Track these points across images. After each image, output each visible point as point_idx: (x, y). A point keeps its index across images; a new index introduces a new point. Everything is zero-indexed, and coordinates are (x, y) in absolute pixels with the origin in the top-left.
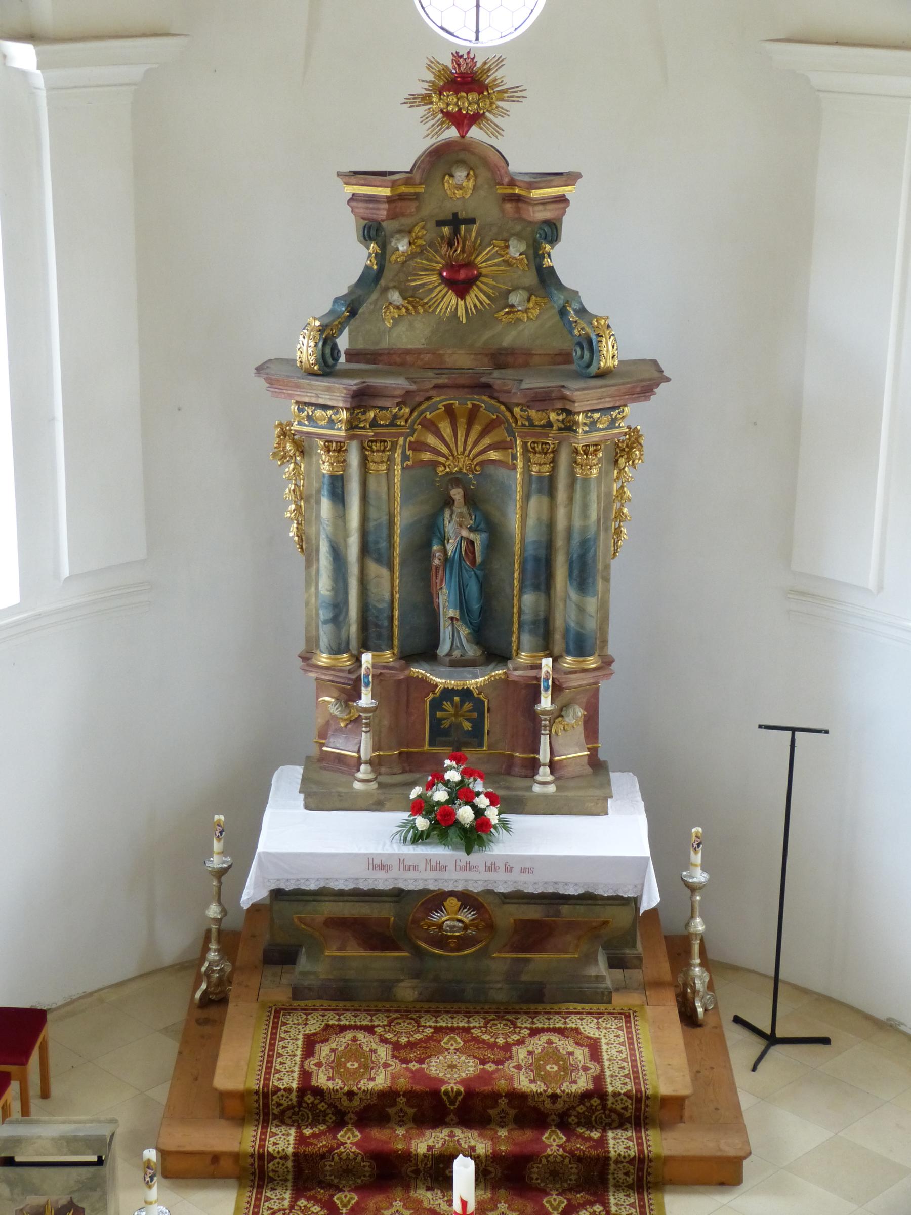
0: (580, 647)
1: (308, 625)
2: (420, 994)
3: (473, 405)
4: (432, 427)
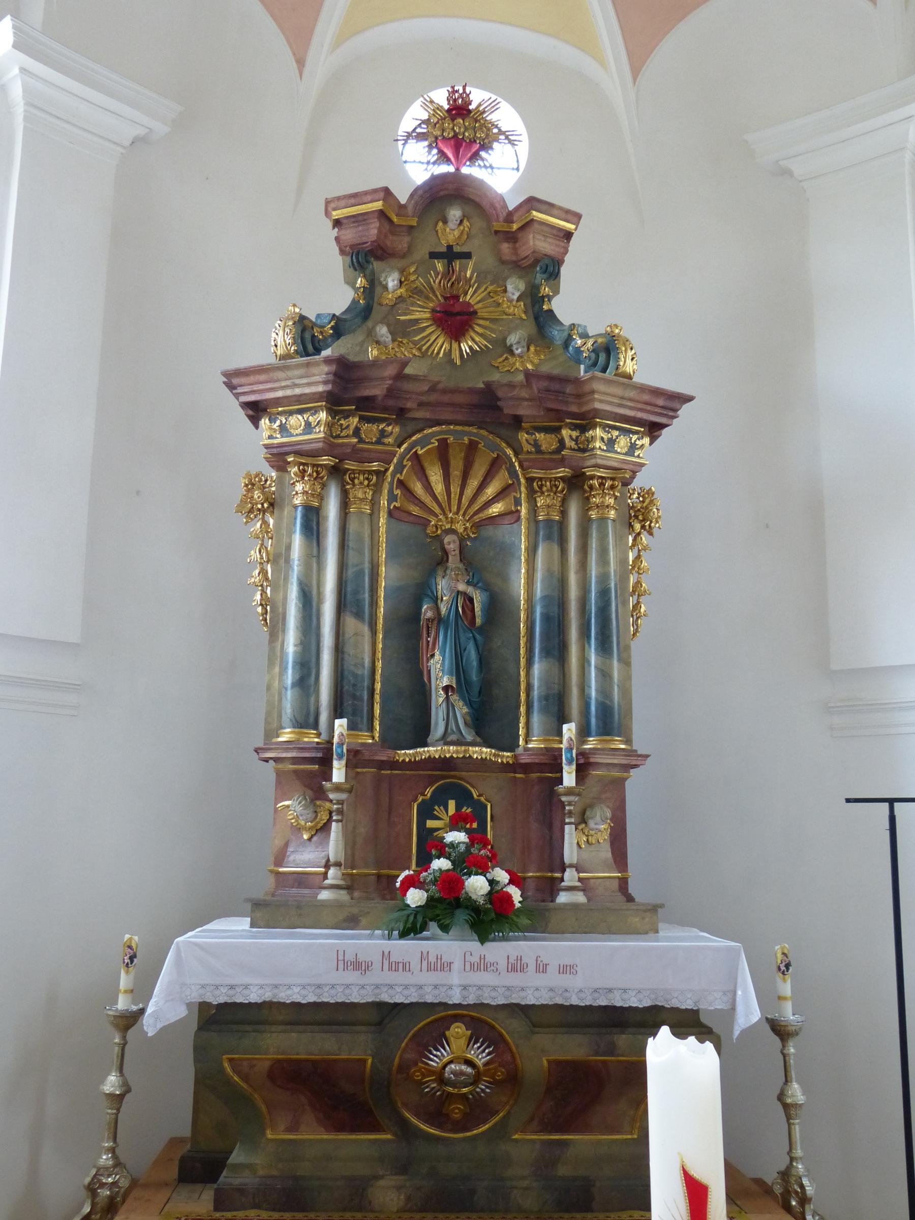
1: (268, 714)
2: (408, 1199)
3: (470, 440)
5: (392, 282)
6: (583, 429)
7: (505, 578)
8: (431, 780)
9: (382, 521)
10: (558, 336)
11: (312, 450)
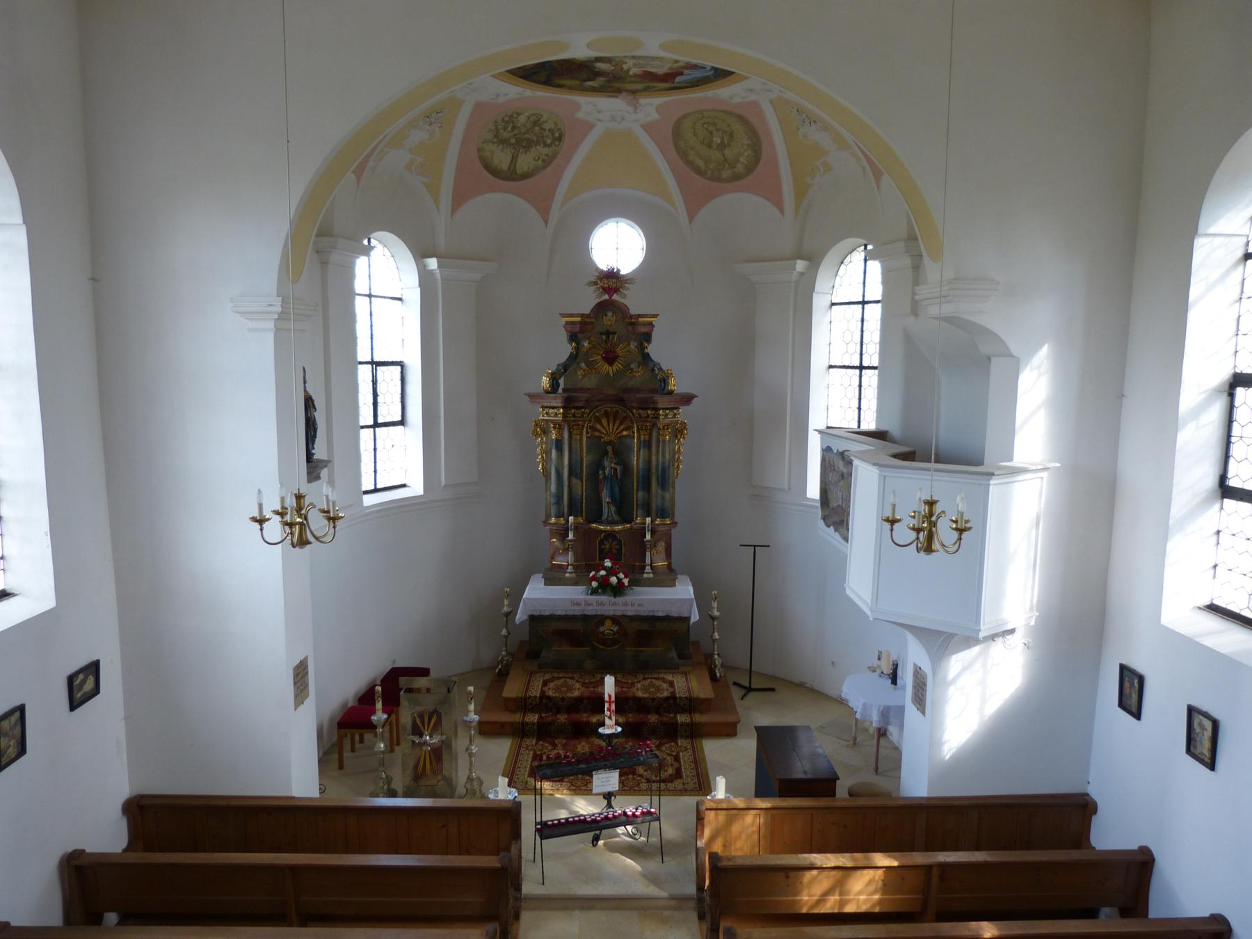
0: (663, 513)
4: (598, 420)
5: (586, 344)
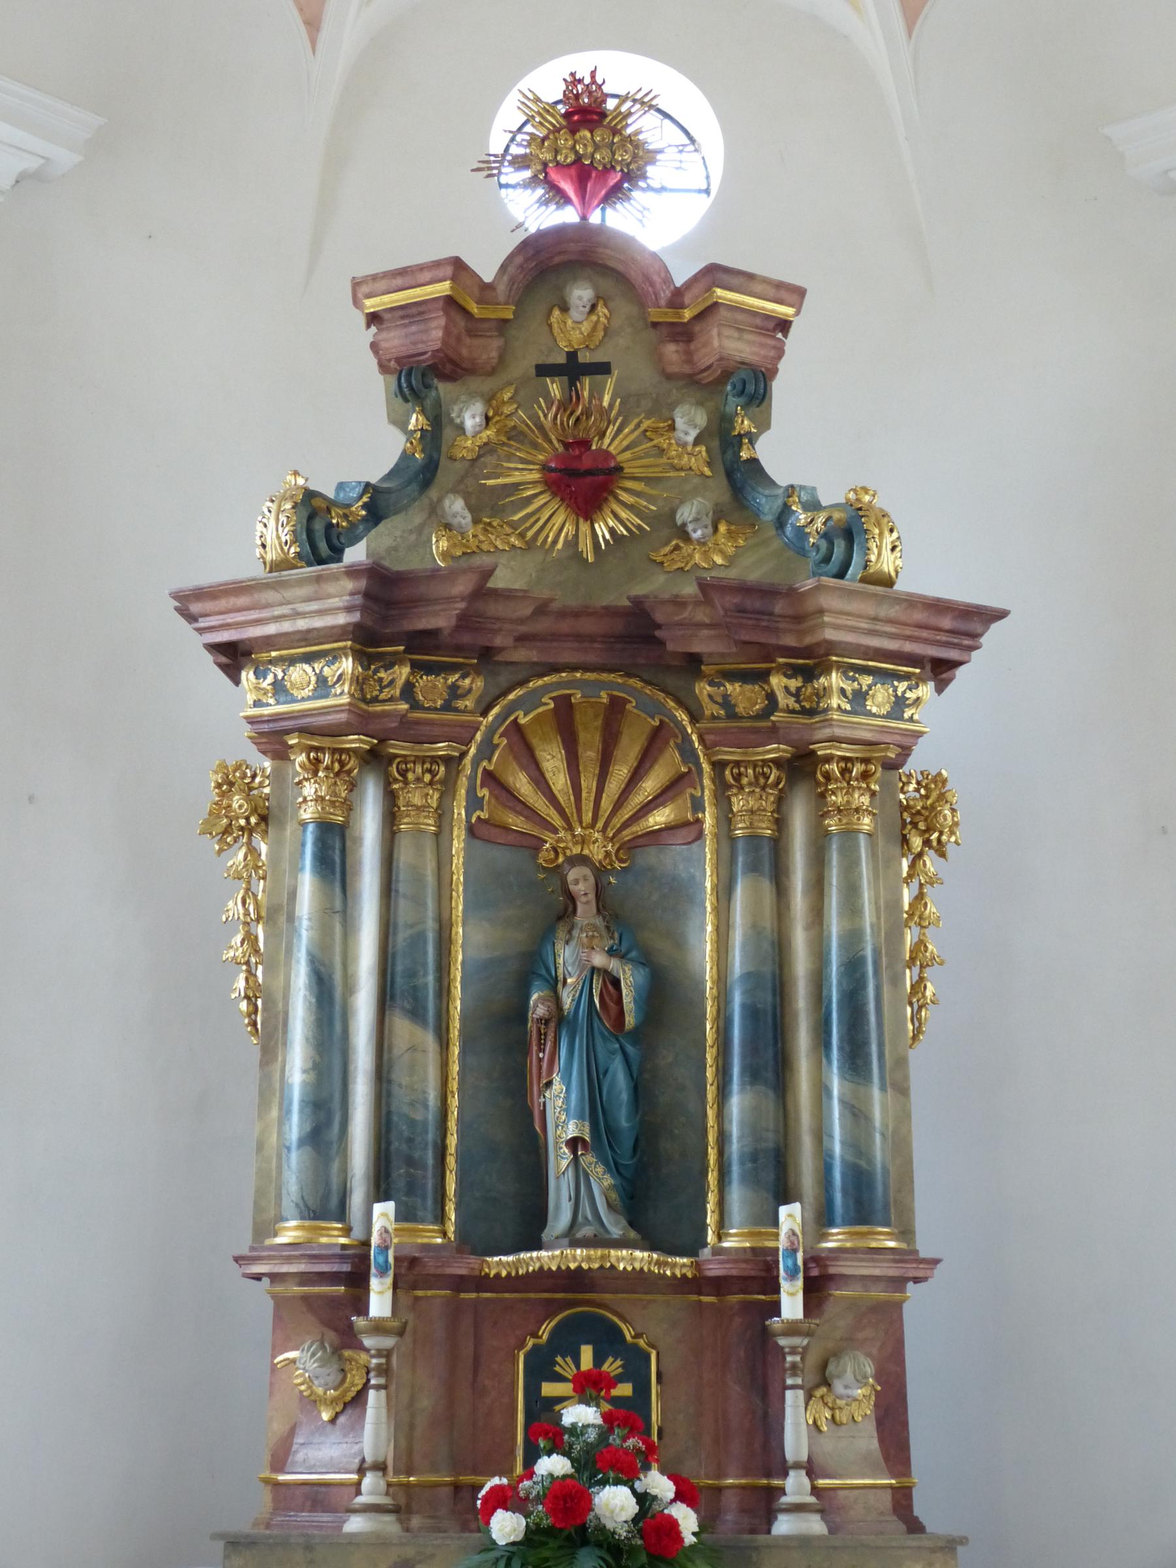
1: (260, 1193)
5: (471, 418)
6: (809, 674)
7: (679, 942)
8: (551, 1308)
9: (458, 844)
10: (768, 507)
11: (330, 726)
